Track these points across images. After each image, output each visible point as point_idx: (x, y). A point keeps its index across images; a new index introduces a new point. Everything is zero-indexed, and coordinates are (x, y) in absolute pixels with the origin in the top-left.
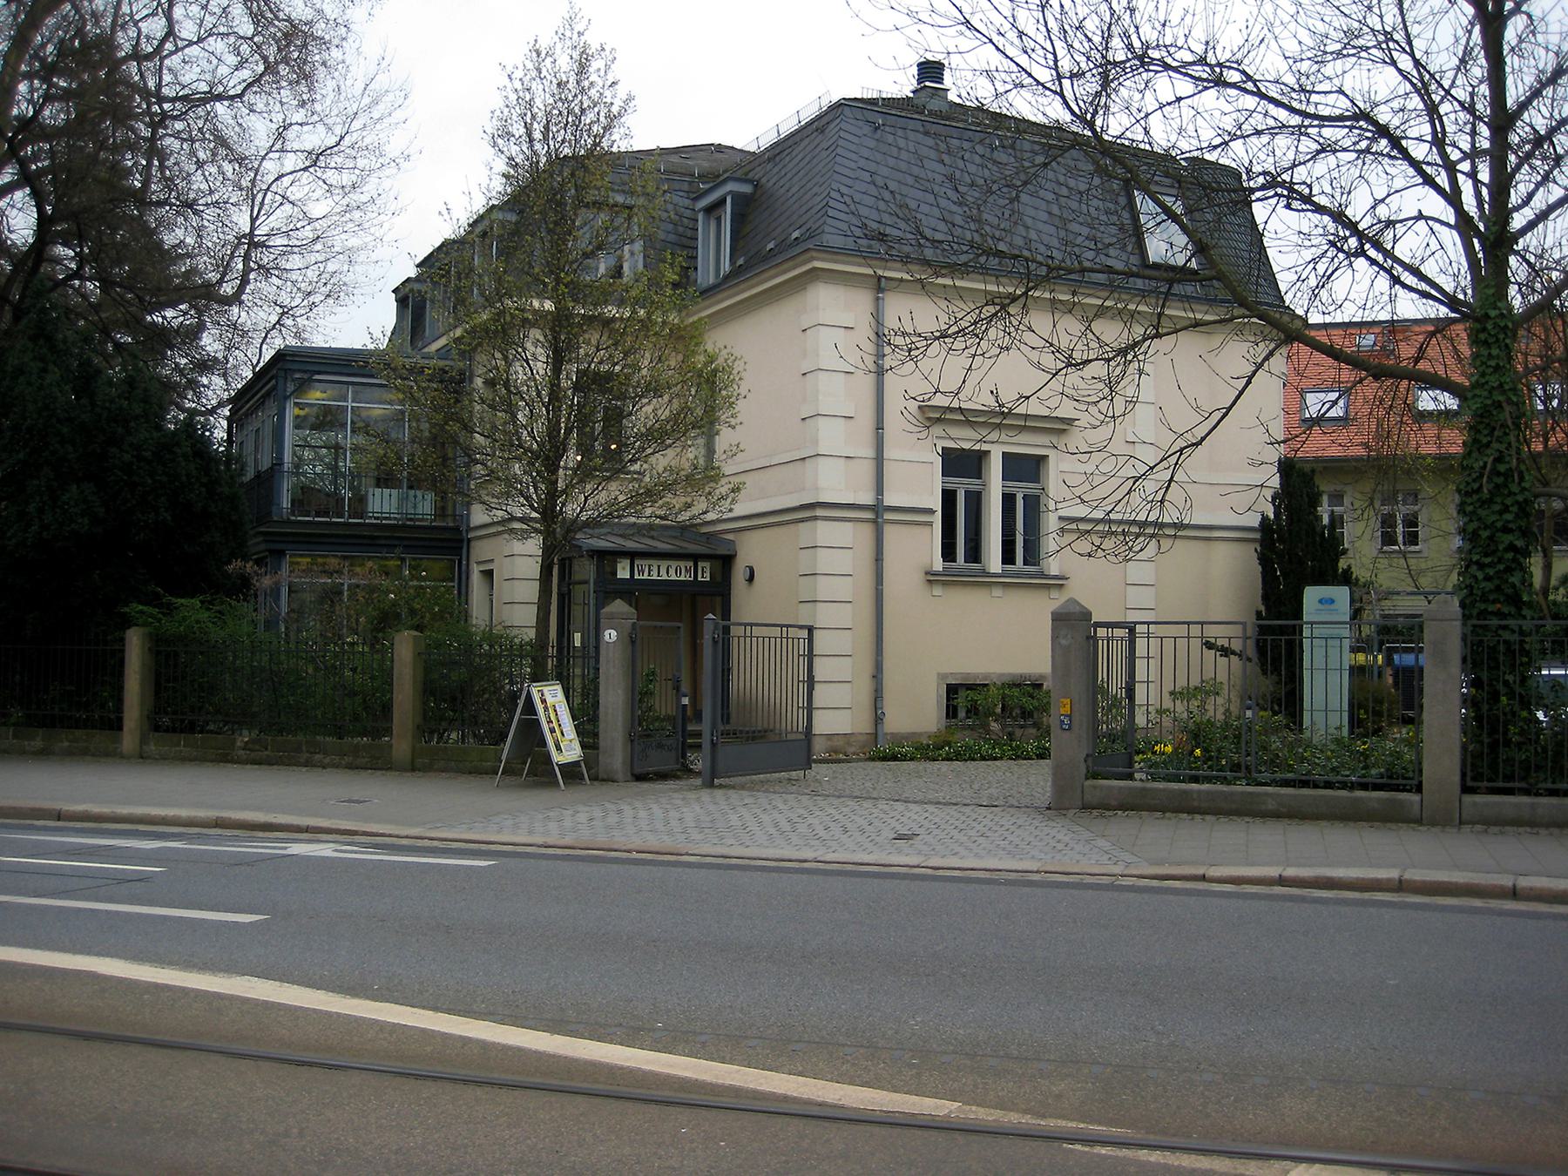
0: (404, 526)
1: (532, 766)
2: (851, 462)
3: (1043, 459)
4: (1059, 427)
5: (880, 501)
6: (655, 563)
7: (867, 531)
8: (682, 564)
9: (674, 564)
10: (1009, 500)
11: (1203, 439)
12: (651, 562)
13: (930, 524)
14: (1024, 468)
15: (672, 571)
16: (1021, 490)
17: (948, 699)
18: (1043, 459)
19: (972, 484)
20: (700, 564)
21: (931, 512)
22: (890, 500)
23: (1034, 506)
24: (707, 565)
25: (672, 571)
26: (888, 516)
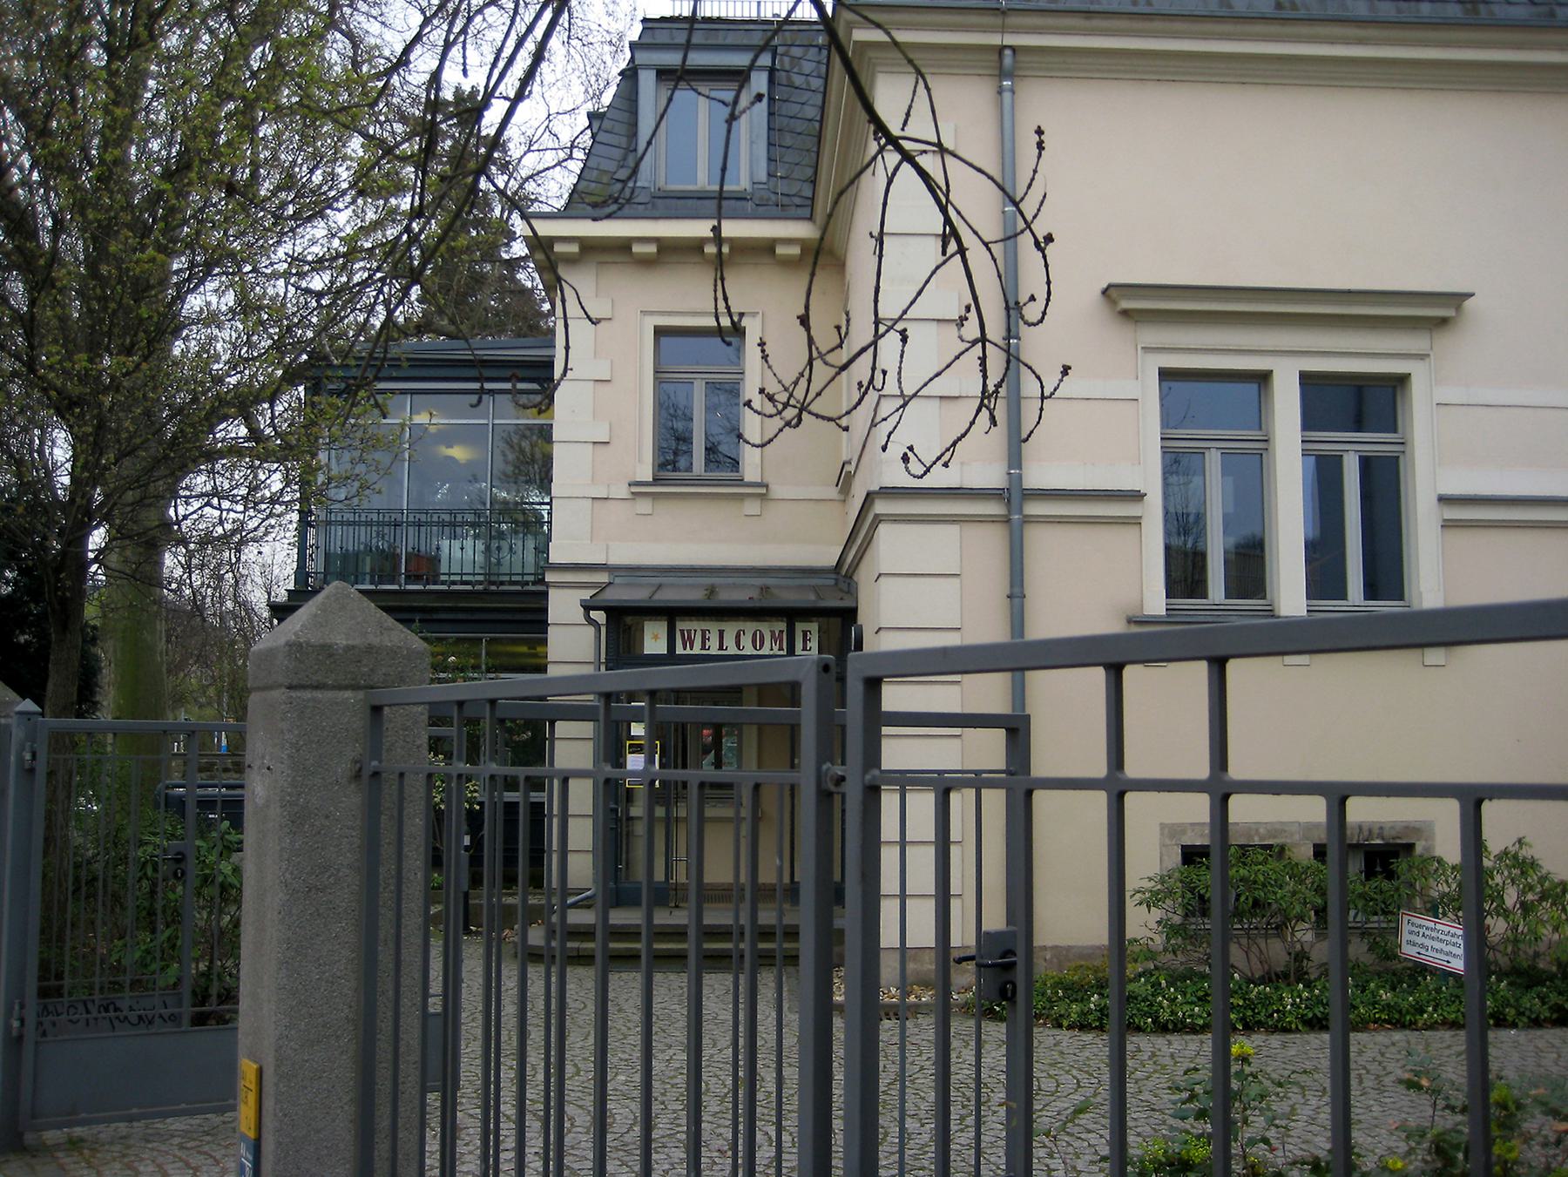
0: (486, 592)
1: (236, 924)
2: (947, 405)
3: (1402, 380)
4: (1435, 313)
5: (1015, 480)
6: (713, 627)
7: (989, 544)
8: (765, 628)
9: (750, 627)
10: (1325, 474)
11: (1044, 313)
12: (740, 625)
13: (1136, 522)
14: (1357, 405)
15: (746, 641)
16: (1351, 450)
17: (1192, 824)
18: (1402, 380)
19: (1374, 442)
20: (800, 627)
21: (1136, 496)
22: (1036, 476)
23: (1384, 480)
24: (813, 627)
25: (746, 641)
26: (1034, 508)
